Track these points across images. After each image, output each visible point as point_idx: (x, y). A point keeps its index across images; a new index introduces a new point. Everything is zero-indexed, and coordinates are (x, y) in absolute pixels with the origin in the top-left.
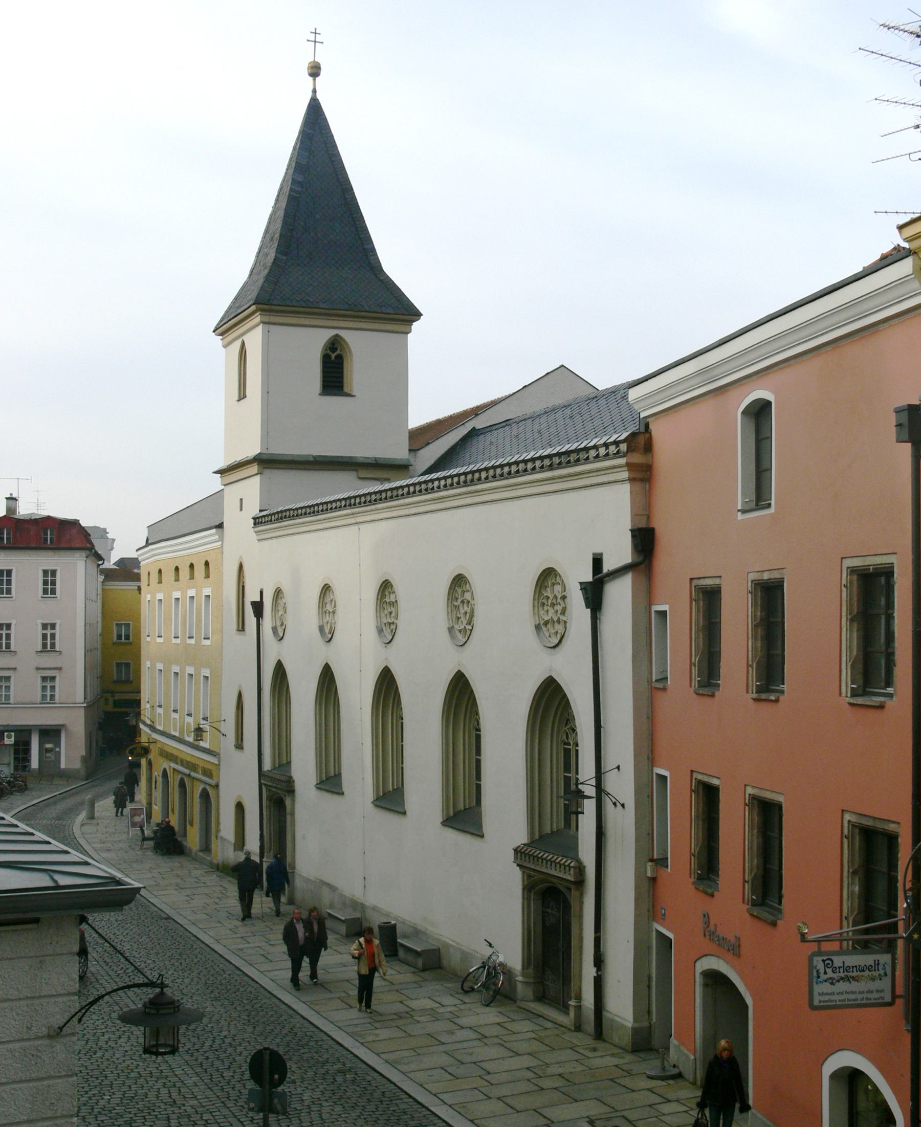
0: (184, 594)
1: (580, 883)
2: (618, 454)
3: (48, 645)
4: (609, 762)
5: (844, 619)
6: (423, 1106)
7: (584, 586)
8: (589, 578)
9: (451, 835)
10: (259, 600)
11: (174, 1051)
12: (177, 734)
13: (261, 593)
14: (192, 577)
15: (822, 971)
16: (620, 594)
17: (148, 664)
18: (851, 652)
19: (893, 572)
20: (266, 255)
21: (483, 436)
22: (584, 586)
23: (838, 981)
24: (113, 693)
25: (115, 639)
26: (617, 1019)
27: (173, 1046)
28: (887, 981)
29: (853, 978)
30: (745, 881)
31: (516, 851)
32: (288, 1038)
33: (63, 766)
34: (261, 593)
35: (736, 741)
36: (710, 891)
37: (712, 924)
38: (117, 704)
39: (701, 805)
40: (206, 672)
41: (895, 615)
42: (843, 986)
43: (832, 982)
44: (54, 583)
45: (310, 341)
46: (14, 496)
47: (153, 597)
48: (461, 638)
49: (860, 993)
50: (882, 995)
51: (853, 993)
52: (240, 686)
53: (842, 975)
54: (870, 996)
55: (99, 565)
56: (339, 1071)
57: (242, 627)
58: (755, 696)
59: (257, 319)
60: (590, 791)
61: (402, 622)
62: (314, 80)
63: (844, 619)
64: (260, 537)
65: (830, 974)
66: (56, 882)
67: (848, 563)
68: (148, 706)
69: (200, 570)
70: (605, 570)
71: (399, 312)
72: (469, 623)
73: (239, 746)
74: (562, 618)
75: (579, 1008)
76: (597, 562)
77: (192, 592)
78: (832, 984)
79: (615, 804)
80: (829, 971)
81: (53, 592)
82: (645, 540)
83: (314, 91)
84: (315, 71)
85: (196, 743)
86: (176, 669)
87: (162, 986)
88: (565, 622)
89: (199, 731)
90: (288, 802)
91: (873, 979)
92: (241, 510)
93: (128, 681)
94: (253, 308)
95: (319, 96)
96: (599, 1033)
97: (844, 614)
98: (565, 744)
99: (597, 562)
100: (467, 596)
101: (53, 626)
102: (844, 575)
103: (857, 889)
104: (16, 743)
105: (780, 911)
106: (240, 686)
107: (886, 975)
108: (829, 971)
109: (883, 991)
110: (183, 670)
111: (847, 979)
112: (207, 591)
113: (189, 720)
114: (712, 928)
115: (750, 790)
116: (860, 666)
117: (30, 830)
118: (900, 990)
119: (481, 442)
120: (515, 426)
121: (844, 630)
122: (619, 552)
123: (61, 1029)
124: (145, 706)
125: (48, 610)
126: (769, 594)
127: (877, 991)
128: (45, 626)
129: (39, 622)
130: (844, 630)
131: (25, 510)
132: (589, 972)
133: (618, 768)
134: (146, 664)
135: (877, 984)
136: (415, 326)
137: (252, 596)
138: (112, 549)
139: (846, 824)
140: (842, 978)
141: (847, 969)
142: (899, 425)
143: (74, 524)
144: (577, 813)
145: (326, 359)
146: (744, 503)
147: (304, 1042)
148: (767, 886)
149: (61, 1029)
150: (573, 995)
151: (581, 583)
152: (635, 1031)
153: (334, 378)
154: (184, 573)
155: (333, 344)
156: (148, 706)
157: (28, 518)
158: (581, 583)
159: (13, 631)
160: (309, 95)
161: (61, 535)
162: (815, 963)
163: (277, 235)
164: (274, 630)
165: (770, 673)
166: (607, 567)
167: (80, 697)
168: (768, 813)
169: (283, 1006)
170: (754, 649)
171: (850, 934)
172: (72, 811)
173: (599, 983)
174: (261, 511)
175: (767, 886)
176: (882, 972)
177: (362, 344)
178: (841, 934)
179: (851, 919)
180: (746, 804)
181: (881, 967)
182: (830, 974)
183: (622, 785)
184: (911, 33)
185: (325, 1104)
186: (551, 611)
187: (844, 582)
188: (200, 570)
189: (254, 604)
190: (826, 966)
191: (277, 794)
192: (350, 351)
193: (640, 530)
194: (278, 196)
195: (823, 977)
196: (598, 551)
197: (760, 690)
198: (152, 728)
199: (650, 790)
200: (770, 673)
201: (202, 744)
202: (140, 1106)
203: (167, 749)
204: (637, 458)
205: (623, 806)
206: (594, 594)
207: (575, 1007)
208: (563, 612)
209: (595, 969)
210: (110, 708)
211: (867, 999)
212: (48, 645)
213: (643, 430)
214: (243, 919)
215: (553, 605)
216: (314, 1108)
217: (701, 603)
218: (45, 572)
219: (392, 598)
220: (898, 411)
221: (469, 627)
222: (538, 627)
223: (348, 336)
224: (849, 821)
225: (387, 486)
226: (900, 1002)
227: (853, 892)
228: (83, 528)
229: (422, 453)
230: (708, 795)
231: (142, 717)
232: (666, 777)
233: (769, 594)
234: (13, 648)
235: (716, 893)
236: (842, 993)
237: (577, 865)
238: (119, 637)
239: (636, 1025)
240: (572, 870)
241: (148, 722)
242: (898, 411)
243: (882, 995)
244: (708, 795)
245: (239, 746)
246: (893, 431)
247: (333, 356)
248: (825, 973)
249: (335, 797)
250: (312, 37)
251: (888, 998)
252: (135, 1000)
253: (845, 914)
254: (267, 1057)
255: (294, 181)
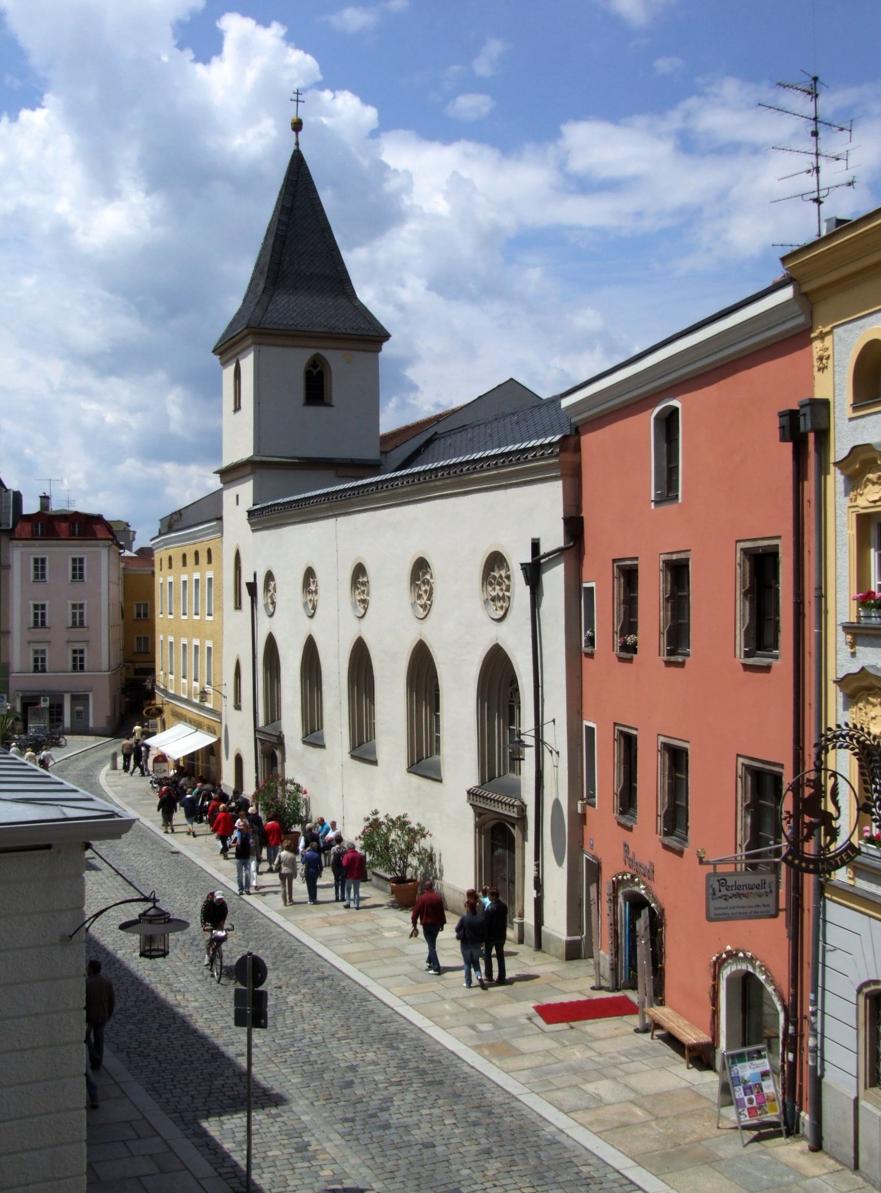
0: (190, 576)
1: (523, 818)
2: (551, 456)
3: (78, 622)
4: (547, 717)
5: (738, 593)
6: (389, 1007)
7: (524, 567)
8: (528, 559)
9: (415, 780)
10: (252, 581)
11: (165, 954)
12: (186, 697)
13: (255, 575)
14: (197, 562)
15: (717, 889)
16: (554, 580)
17: (161, 637)
18: (744, 620)
19: (777, 553)
20: (257, 285)
21: (442, 440)
22: (524, 567)
23: (731, 897)
24: (133, 662)
25: (135, 617)
26: (553, 933)
27: (164, 950)
28: (772, 897)
29: (744, 895)
30: (657, 815)
31: (469, 792)
32: (276, 951)
33: (91, 725)
34: (255, 575)
35: (649, 698)
36: (629, 824)
37: (631, 853)
38: (137, 672)
39: (622, 752)
40: (209, 643)
41: (780, 588)
42: (734, 902)
43: (726, 898)
44: (81, 569)
45: (297, 360)
46: (47, 494)
47: (165, 579)
48: (421, 613)
49: (749, 907)
50: (768, 909)
51: (743, 907)
52: (238, 655)
53: (734, 892)
54: (758, 909)
55: (120, 553)
56: (319, 978)
57: (238, 606)
58: (666, 658)
59: (250, 341)
60: (530, 740)
61: (373, 600)
62: (297, 134)
63: (738, 593)
64: (635, 562)
65: (724, 891)
66: (64, 814)
67: (741, 545)
68: (162, 673)
69: (203, 558)
70: (542, 553)
71: (372, 336)
72: (429, 599)
73: (238, 707)
74: (507, 594)
75: (521, 926)
76: (535, 546)
77: (197, 576)
78: (725, 899)
79: (551, 752)
80: (723, 889)
81: (81, 577)
82: (574, 526)
83: (297, 144)
84: (297, 126)
85: (202, 704)
86: (184, 641)
87: (155, 900)
88: (509, 598)
89: (203, 694)
90: (278, 753)
91: (760, 896)
92: (237, 504)
93: (147, 653)
94: (246, 332)
95: (301, 148)
96: (539, 946)
97: (738, 588)
98: (510, 701)
99: (535, 546)
100: (428, 577)
101: (81, 606)
102: (738, 555)
103: (749, 820)
104: (51, 706)
105: (686, 840)
106: (238, 655)
107: (771, 892)
108: (723, 889)
109: (769, 905)
110: (190, 642)
111: (738, 896)
112: (210, 574)
113: (196, 685)
114: (631, 856)
115: (662, 739)
116: (753, 633)
117: (60, 780)
118: (782, 904)
119: (439, 446)
120: (470, 430)
121: (738, 602)
122: (554, 538)
123: (71, 937)
124: (160, 673)
125: (41, 593)
126: (678, 572)
127: (764, 906)
128: (74, 606)
129: (70, 602)
130: (738, 602)
131: (55, 507)
132: (530, 894)
133: (554, 721)
134: (160, 637)
135: (764, 900)
136: (385, 345)
137: (246, 578)
138: (134, 539)
139: (740, 766)
140: (734, 895)
141: (738, 887)
142: (782, 428)
143: (98, 519)
144: (520, 760)
145: (309, 375)
146: (656, 495)
147: (289, 955)
148: (675, 819)
149: (71, 937)
150: (517, 914)
151: (522, 564)
152: (569, 944)
153: (316, 389)
154: (191, 559)
155: (315, 362)
156: (162, 673)
157: (59, 513)
158: (522, 564)
159: (47, 611)
160: (293, 148)
161: (86, 527)
162: (711, 883)
163: (266, 269)
164: (266, 606)
165: (677, 637)
166: (544, 549)
167: (105, 665)
168: (676, 758)
169: (274, 925)
170: (665, 618)
171: (744, 858)
172: (100, 763)
173: (539, 903)
174: (254, 505)
175: (675, 819)
176: (768, 890)
177: (337, 360)
178: (736, 858)
179: (744, 846)
180: (615, 740)
181: (767, 885)
182: (724, 891)
183: (557, 736)
184: (804, 91)
185: (305, 1005)
186: (498, 588)
187: (738, 561)
188: (203, 558)
189: (248, 584)
190: (721, 885)
191: (270, 749)
192: (329, 367)
193: (571, 518)
194: (267, 235)
195: (718, 894)
196: (536, 537)
197: (671, 653)
198: (165, 692)
199: (580, 741)
200: (677, 637)
201: (207, 705)
202: (151, 1007)
203: (178, 709)
204: (568, 457)
205: (558, 753)
206: (533, 573)
207: (519, 924)
208: (508, 590)
209: (535, 892)
210: (132, 676)
211: (755, 912)
212: (78, 622)
213: (573, 433)
214: (411, 936)
215: (499, 584)
216: (296, 1009)
217: (622, 580)
218: (74, 560)
219: (365, 579)
220: (781, 415)
221: (429, 602)
222: (486, 602)
223: (326, 354)
224: (662, 743)
225: (360, 483)
226: (782, 915)
227: (745, 823)
228: (106, 522)
229: (393, 454)
230: (629, 743)
231: (157, 683)
232: (593, 729)
233: (678, 572)
234: (47, 624)
235: (634, 826)
236: (734, 908)
237: (520, 804)
238: (139, 615)
239: (570, 938)
240: (516, 809)
241: (162, 687)
242: (781, 415)
243: (768, 909)
244: (629, 743)
245: (238, 707)
246: (776, 433)
247: (315, 372)
248: (720, 891)
249: (318, 750)
250: (295, 97)
251: (773, 912)
252: (135, 911)
253: (739, 842)
254: (249, 963)
255: (280, 222)
